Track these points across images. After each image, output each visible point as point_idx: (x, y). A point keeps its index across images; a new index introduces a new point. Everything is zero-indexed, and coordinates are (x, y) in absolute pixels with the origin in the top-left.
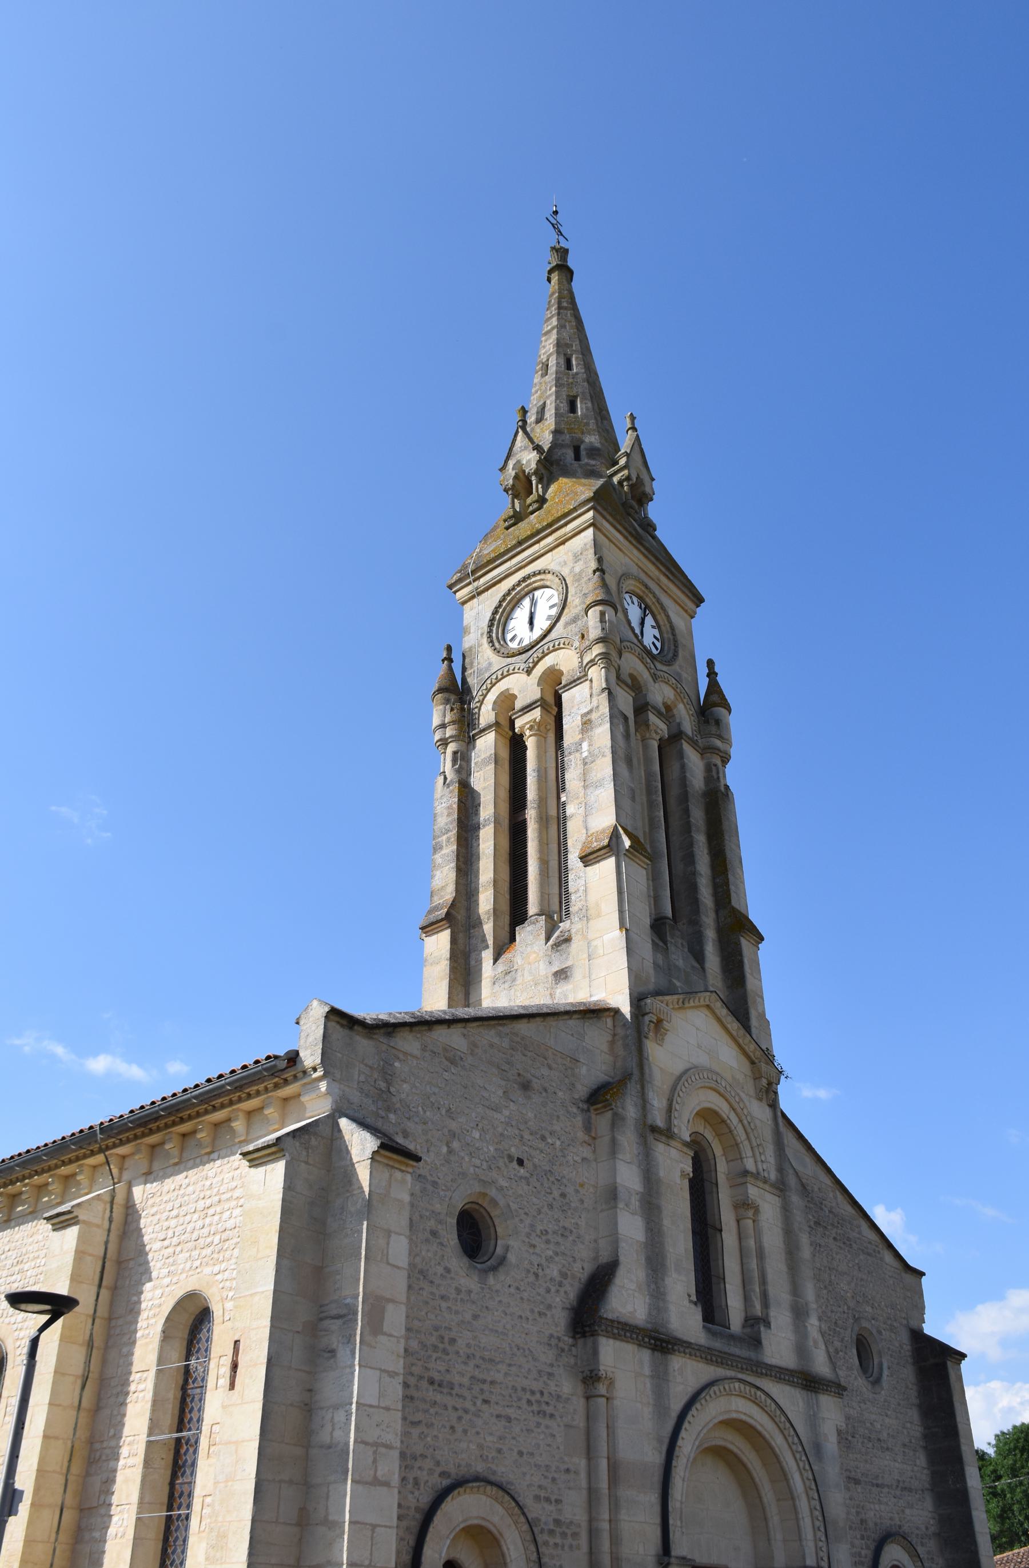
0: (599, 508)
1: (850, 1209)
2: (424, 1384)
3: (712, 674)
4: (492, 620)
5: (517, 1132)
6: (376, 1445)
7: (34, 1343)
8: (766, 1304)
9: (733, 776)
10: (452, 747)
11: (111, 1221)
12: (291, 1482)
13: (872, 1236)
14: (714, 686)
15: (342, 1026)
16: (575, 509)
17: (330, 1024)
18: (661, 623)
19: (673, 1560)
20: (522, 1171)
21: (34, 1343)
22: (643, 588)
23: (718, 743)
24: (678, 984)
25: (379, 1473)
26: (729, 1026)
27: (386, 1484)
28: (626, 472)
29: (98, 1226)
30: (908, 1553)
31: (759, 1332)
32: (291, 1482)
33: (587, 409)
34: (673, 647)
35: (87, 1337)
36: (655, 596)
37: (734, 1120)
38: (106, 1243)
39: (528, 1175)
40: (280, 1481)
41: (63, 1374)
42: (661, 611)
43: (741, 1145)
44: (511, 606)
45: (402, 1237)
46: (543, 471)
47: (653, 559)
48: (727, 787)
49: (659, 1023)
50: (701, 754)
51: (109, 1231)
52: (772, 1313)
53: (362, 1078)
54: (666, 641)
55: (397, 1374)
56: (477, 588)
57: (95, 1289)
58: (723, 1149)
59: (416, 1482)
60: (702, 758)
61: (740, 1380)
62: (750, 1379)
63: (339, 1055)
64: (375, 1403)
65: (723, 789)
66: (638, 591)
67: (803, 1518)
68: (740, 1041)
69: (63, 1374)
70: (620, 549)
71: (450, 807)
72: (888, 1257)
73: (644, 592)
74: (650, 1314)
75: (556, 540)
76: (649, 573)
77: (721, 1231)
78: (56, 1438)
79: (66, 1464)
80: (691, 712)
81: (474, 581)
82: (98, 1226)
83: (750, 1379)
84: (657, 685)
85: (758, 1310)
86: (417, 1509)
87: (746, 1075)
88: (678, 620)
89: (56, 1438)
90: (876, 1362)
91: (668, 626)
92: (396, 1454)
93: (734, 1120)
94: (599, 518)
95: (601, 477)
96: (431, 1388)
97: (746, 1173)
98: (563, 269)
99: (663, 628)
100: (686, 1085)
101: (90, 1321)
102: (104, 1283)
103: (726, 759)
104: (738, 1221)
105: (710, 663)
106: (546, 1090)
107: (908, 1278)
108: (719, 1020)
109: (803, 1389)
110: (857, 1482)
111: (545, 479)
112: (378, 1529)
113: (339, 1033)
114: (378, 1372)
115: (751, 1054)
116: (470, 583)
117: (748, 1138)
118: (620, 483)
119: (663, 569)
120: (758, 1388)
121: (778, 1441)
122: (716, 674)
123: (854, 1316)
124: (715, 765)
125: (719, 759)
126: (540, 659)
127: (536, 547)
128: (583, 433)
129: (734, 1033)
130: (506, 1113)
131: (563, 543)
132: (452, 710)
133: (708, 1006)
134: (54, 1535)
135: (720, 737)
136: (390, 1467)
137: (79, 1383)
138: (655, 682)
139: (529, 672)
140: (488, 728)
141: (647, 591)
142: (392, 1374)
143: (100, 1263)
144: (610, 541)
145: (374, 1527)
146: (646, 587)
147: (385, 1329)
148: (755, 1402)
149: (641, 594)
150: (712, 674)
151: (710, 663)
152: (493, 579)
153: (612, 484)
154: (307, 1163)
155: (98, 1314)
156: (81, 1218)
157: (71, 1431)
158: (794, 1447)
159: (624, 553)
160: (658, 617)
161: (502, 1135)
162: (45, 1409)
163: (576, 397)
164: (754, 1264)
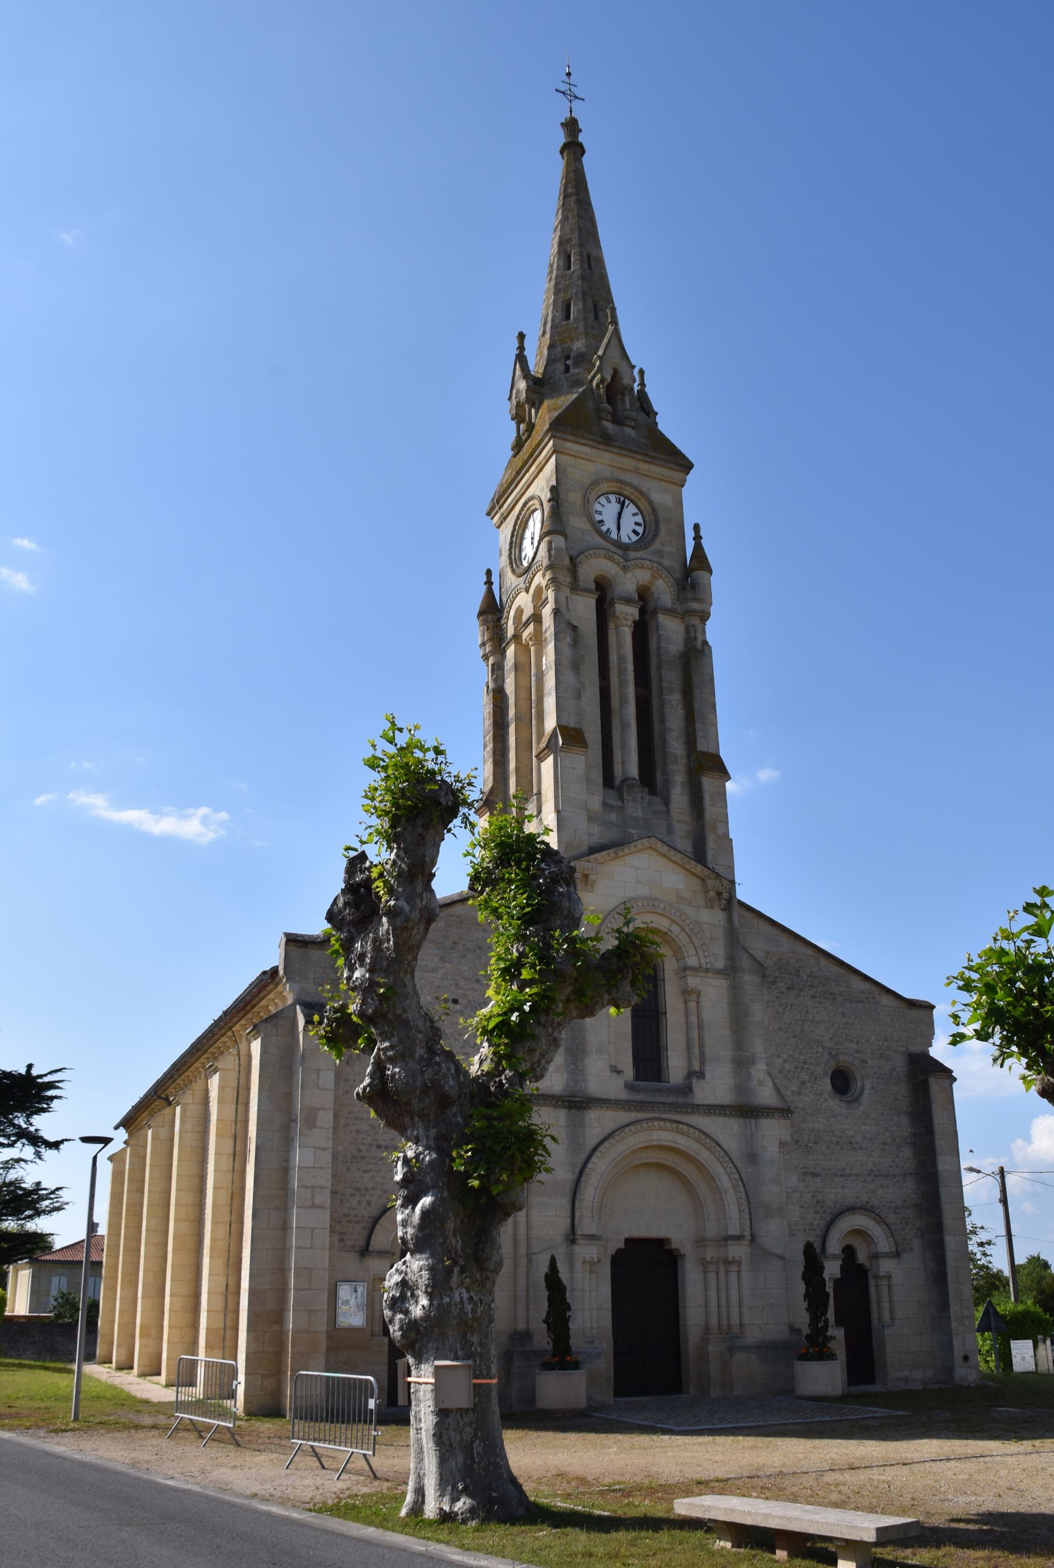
0: (558, 435)
1: (837, 969)
2: (374, 1149)
3: (698, 538)
4: (511, 543)
5: (452, 982)
6: (313, 1187)
7: (95, 1159)
8: (702, 1061)
9: (714, 632)
10: (491, 660)
11: (239, 1065)
12: (276, 1208)
13: (867, 986)
14: (698, 548)
15: (299, 947)
16: (542, 440)
17: (289, 948)
18: (642, 508)
19: (577, 1237)
20: (458, 1007)
21: (95, 1159)
22: (618, 485)
23: (695, 605)
24: (633, 831)
25: (316, 1202)
26: (673, 858)
27: (322, 1207)
28: (599, 376)
29: (231, 1070)
30: (874, 1220)
31: (691, 1083)
32: (276, 1208)
33: (578, 311)
34: (653, 527)
35: (233, 1133)
36: (631, 485)
37: (676, 929)
38: (238, 1079)
39: (462, 1009)
40: (269, 1209)
41: (221, 1154)
42: (640, 497)
43: (683, 948)
44: (522, 528)
45: (329, 1072)
46: (534, 396)
47: (628, 453)
48: (705, 643)
49: (586, 876)
50: (682, 618)
51: (239, 1071)
52: (708, 1068)
53: (317, 976)
54: (648, 524)
55: (327, 1148)
56: (502, 514)
57: (234, 1106)
58: (674, 952)
59: (369, 1203)
60: (683, 622)
61: (659, 1119)
62: (676, 1117)
63: (298, 966)
64: (312, 1165)
65: (699, 645)
66: (614, 489)
67: (728, 1205)
68: (687, 866)
69: (221, 1154)
70: (589, 460)
71: (489, 713)
72: (886, 1000)
73: (620, 488)
74: (567, 1085)
75: (537, 467)
76: (625, 467)
77: (666, 1013)
78: (221, 1188)
79: (229, 1201)
80: (670, 584)
81: (500, 509)
82: (231, 1070)
83: (676, 1117)
84: (629, 575)
85: (696, 1066)
86: (369, 1217)
87: (694, 892)
88: (660, 497)
89: (221, 1188)
90: (859, 1084)
91: (649, 508)
92: (328, 1191)
93: (676, 929)
94: (560, 442)
95: (582, 385)
96: (379, 1150)
97: (685, 969)
98: (573, 149)
99: (645, 512)
100: (613, 920)
101: (234, 1124)
102: (240, 1101)
103: (705, 617)
104: (686, 1003)
105: (697, 527)
106: (480, 948)
107: (915, 1013)
108: (664, 856)
109: (739, 1117)
110: (814, 1175)
111: (537, 403)
112: (316, 1231)
113: (296, 951)
114: (313, 1150)
115: (700, 874)
116: (497, 512)
117: (692, 941)
118: (598, 386)
119: (640, 457)
120: (679, 1122)
121: (704, 1155)
122: (701, 538)
123: (831, 1054)
124: (694, 626)
125: (698, 618)
126: (532, 579)
127: (527, 475)
128: (572, 341)
129: (680, 862)
130: (442, 971)
131: (541, 470)
132: (488, 629)
133: (650, 848)
134: (228, 1237)
135: (696, 600)
136: (324, 1198)
137: (232, 1158)
138: (625, 573)
139: (527, 591)
140: (511, 640)
141: (622, 486)
142: (324, 1149)
143: (236, 1092)
144: (576, 457)
145: (313, 1229)
146: (621, 482)
147: (318, 1124)
148: (678, 1131)
149: (617, 490)
150: (698, 538)
151: (697, 527)
152: (510, 505)
153: (592, 389)
154: (277, 1035)
155: (238, 1119)
156: (219, 1067)
157: (230, 1184)
158: (721, 1159)
159: (593, 461)
160: (639, 504)
161: (438, 987)
162: (213, 1173)
163: (570, 300)
164: (695, 1034)
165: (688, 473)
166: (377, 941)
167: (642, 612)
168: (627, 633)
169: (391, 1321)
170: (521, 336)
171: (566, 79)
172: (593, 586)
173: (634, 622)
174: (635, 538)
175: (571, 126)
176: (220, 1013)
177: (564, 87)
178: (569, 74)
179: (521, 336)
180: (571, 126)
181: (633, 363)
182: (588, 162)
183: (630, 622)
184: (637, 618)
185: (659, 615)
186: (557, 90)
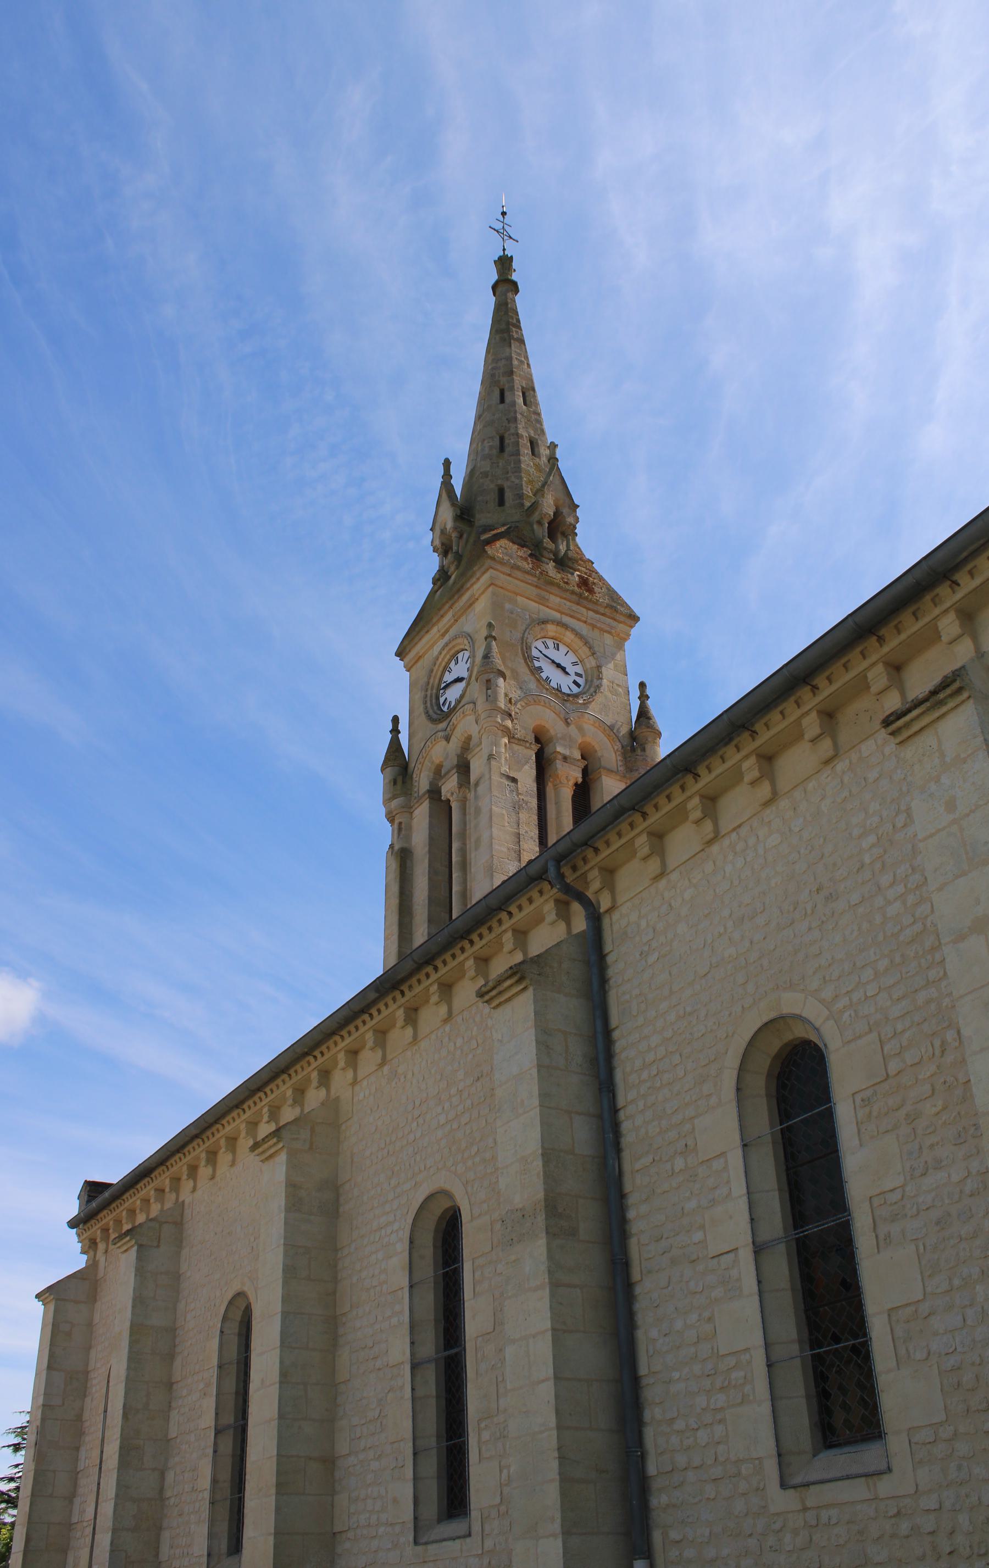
3: (643, 697)
52: (791, 1491)
80: (616, 748)
105: (642, 685)
150: (643, 697)
151: (642, 685)
165: (632, 627)
166: (17, 1448)
167: (585, 772)
168: (567, 793)
169: (513, 482)
170: (447, 463)
171: (501, 218)
172: (531, 738)
173: (576, 784)
174: (575, 690)
175: (504, 263)
176: (80, 1249)
177: (499, 226)
178: (504, 214)
179: (447, 463)
180: (504, 263)
181: (576, 502)
182: (521, 302)
183: (571, 783)
184: (580, 780)
185: (604, 777)
186: (490, 227)
